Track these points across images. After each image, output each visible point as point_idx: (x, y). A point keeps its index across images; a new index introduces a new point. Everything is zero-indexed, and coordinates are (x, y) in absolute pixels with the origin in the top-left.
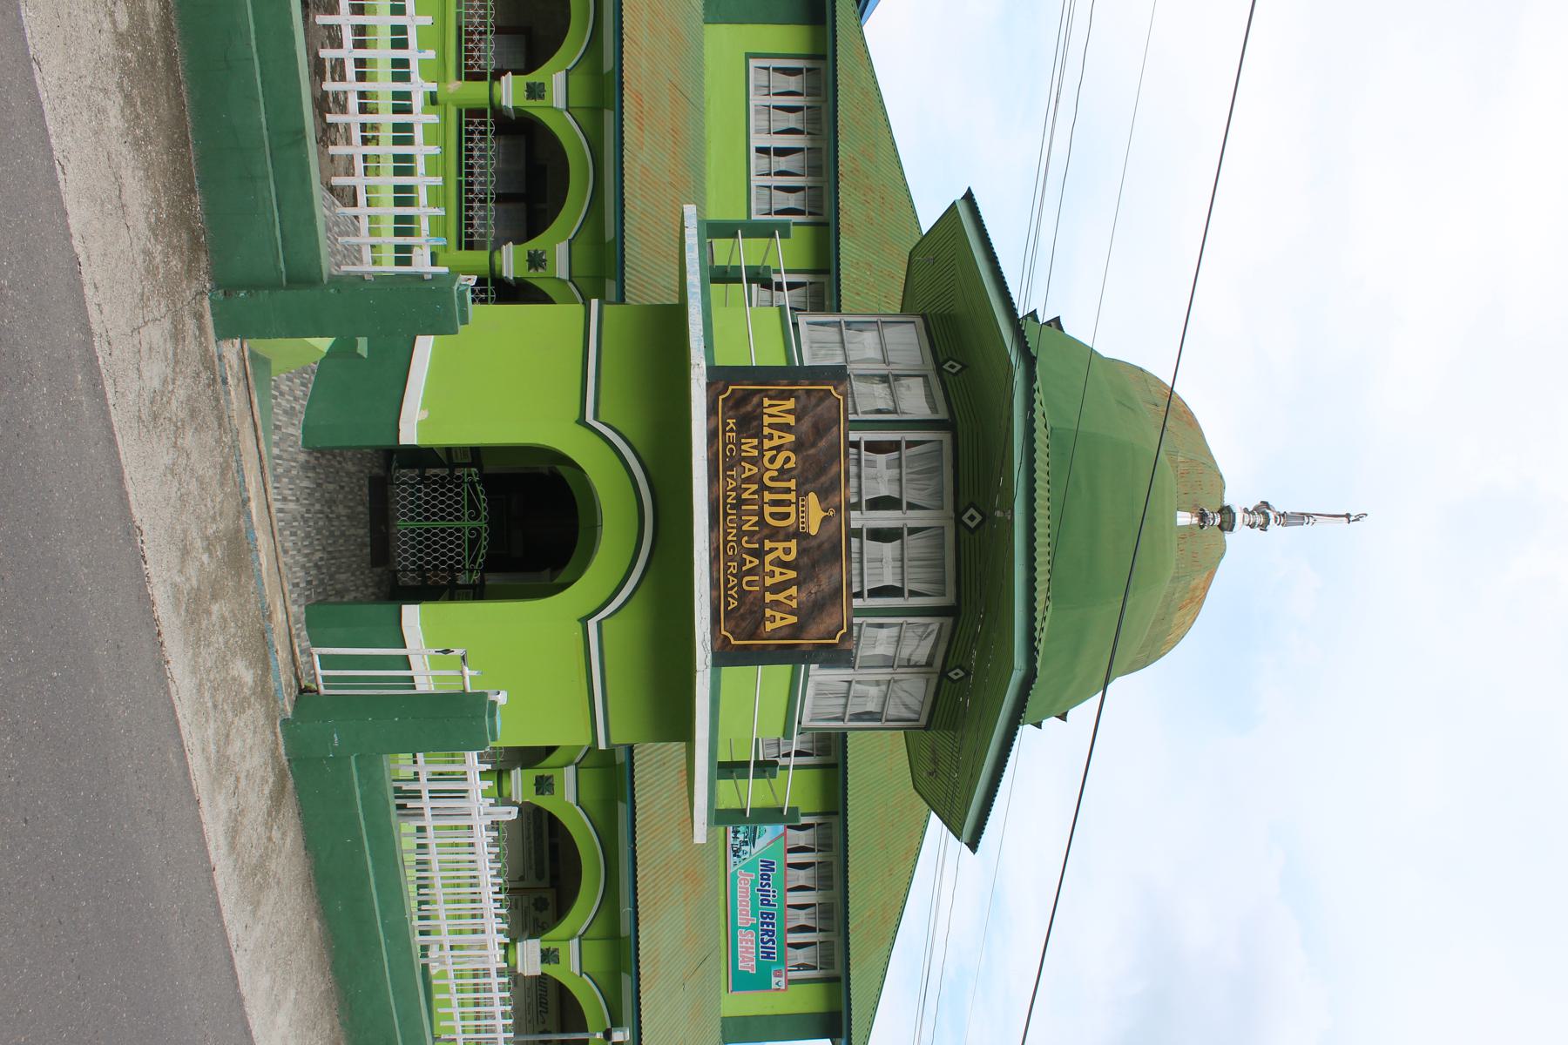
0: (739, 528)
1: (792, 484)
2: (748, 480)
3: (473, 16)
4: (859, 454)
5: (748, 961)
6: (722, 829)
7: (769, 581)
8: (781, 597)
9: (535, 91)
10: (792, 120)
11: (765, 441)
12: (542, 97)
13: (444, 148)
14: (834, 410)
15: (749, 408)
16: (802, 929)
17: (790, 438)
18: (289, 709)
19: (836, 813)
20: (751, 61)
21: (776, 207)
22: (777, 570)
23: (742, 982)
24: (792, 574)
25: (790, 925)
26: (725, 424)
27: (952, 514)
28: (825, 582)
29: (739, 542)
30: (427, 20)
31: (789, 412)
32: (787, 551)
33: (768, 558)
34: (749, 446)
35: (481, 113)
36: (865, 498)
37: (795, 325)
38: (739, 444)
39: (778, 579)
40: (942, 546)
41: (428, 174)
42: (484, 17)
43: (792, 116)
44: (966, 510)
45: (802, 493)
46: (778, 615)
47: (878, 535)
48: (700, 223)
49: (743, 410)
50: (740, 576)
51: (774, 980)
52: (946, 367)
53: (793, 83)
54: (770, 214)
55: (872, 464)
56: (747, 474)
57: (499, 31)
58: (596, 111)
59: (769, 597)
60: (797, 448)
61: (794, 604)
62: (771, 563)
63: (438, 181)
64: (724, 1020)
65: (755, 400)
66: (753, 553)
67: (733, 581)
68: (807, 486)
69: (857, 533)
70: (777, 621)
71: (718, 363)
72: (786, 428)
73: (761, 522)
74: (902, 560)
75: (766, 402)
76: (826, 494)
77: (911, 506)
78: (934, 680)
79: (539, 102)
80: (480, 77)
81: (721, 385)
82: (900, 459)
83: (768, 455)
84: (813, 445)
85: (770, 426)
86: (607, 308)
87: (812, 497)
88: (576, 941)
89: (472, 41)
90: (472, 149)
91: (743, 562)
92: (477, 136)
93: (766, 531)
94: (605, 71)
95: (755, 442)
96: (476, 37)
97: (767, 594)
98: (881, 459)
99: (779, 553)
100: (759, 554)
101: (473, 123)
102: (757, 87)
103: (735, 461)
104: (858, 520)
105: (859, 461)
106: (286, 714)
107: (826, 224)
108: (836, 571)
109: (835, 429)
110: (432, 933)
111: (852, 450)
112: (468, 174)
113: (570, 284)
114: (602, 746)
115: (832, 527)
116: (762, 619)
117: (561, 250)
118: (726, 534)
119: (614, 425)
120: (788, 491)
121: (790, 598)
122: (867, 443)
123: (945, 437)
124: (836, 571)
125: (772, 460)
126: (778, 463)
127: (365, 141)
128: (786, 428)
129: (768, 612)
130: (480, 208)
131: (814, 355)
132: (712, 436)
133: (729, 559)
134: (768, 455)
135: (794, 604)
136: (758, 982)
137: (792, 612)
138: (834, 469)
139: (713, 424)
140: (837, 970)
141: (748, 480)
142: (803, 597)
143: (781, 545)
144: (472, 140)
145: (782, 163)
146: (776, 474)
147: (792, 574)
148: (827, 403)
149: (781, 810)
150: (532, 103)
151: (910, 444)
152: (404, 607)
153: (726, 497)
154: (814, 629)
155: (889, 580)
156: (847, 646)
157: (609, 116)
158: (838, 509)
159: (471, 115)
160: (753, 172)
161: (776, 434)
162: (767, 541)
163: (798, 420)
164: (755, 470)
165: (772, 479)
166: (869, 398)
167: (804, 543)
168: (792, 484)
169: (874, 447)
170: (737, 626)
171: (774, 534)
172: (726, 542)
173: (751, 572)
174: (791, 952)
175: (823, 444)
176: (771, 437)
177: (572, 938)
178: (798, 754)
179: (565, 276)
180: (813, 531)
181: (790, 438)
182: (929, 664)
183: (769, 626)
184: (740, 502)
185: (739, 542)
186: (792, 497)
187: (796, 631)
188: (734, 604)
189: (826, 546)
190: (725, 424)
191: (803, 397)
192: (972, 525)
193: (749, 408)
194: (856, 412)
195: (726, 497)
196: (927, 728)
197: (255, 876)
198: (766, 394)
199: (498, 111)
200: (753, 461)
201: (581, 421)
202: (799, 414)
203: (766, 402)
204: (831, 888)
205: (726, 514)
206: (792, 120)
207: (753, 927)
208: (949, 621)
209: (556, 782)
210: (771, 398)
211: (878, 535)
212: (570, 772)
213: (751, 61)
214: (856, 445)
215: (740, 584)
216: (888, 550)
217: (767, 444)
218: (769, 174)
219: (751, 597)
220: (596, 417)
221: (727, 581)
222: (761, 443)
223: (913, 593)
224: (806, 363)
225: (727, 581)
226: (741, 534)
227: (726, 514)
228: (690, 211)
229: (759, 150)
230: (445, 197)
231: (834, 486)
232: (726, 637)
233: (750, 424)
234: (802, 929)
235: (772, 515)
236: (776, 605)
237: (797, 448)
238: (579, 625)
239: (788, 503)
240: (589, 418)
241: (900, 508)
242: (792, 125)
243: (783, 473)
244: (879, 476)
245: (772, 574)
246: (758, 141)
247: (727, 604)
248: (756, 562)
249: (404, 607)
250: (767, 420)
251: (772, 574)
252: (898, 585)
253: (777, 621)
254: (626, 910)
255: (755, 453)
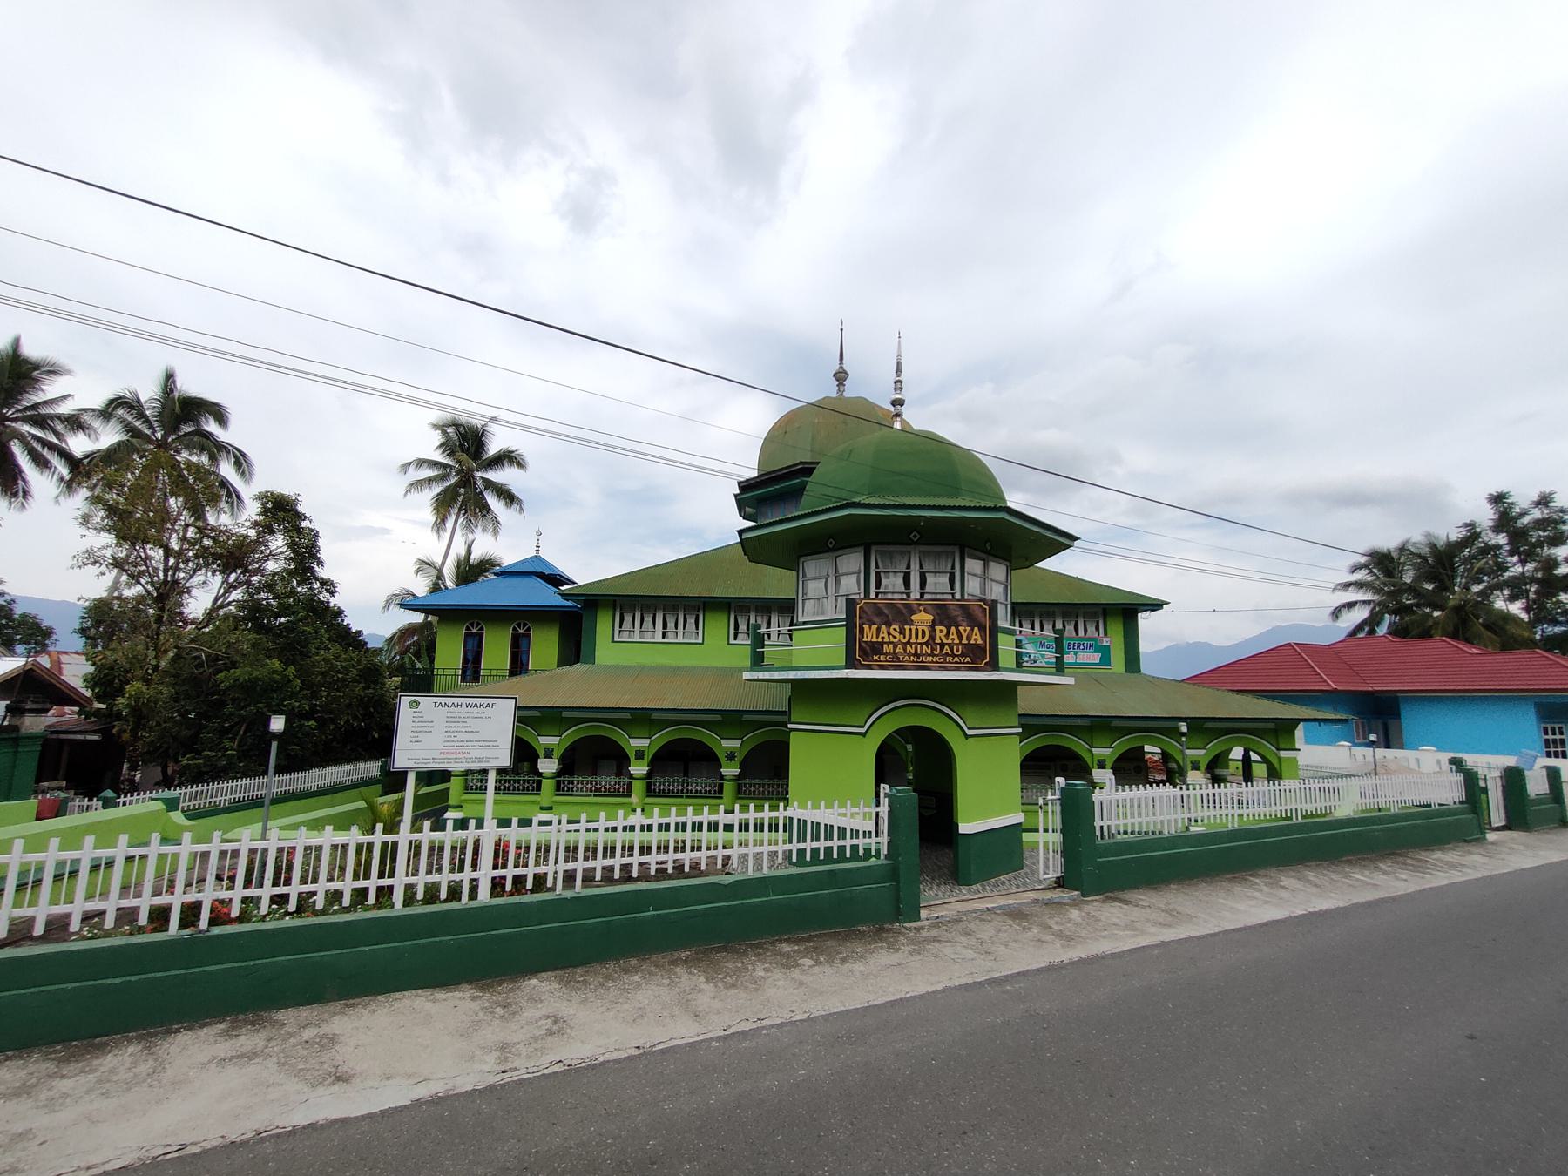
0: (929, 655)
1: (907, 627)
2: (905, 650)
3: (750, 791)
4: (881, 593)
5: (1096, 658)
6: (1066, 670)
7: (957, 641)
8: (965, 635)
9: (640, 755)
10: (648, 619)
11: (885, 640)
12: (643, 751)
13: (674, 805)
14: (869, 605)
15: (868, 648)
16: (1097, 629)
17: (883, 627)
18: (1076, 893)
19: (615, 601)
20: (615, 640)
21: (694, 629)
22: (951, 637)
23: (1106, 661)
24: (953, 629)
25: (1074, 634)
26: (876, 661)
27: (912, 546)
28: (957, 612)
29: (936, 656)
30: (603, 815)
31: (870, 628)
32: (941, 631)
33: (945, 641)
34: (888, 649)
35: (558, 783)
36: (904, 591)
37: (805, 623)
38: (886, 654)
39: (955, 636)
40: (929, 552)
41: (686, 815)
42: (778, 785)
43: (645, 619)
44: (910, 539)
45: (911, 623)
46: (974, 637)
47: (923, 584)
48: (752, 670)
49: (869, 651)
50: (954, 656)
51: (1105, 644)
52: (831, 546)
53: (628, 618)
54: (697, 633)
55: (886, 587)
56: (902, 650)
57: (594, 773)
58: (742, 724)
59: (965, 641)
60: (889, 625)
61: (968, 629)
62: (947, 639)
63: (674, 809)
64: (1126, 671)
65: (864, 645)
66: (942, 650)
67: (956, 659)
68: (908, 620)
69: (922, 595)
70: (977, 637)
71: (844, 664)
72: (878, 630)
73: (926, 644)
74: (936, 573)
75: (865, 639)
76: (911, 610)
77: (908, 567)
78: (991, 557)
79: (646, 753)
80: (721, 787)
81: (856, 662)
82: (884, 572)
83: (892, 639)
84: (887, 616)
85: (877, 637)
86: (792, 720)
87: (913, 618)
88: (1093, 749)
89: (610, 788)
90: (660, 790)
91: (947, 654)
92: (526, 785)
93: (931, 641)
94: (721, 719)
95: (885, 646)
96: (598, 786)
97: (963, 642)
98: (884, 581)
99: (942, 635)
100: (942, 645)
101: (563, 788)
102: (630, 637)
103: (895, 657)
104: (915, 594)
105: (885, 593)
106: (1078, 895)
107: (704, 603)
108: (951, 607)
109: (880, 605)
110: (480, 816)
111: (880, 596)
112: (682, 792)
113: (563, 736)
114: (1020, 730)
115: (929, 608)
116: (976, 645)
117: (725, 743)
118: (932, 662)
119: (867, 716)
120: (910, 630)
121: (965, 631)
122: (876, 588)
123: (874, 548)
124: (951, 607)
125: (895, 637)
126: (897, 634)
127: (747, 845)
128: (878, 630)
129: (972, 642)
130: (692, 786)
131: (841, 612)
132: (882, 667)
133: (945, 662)
134: (892, 639)
135: (968, 629)
136: (1106, 652)
137: (972, 630)
138: (899, 606)
139: (876, 667)
140: (1100, 610)
141: (905, 650)
142: (964, 624)
143: (938, 634)
144: (710, 791)
145: (671, 625)
146: (902, 636)
147: (953, 629)
148: (866, 609)
149: (1056, 638)
150: (646, 757)
151: (877, 567)
152: (960, 832)
153: (913, 662)
154: (981, 619)
155: (945, 579)
156: (990, 602)
157: (655, 716)
158: (920, 605)
159: (650, 790)
160: (652, 640)
161: (881, 635)
162: (936, 641)
163: (874, 624)
164: (899, 646)
165: (904, 637)
166: (851, 585)
167: (937, 622)
168: (907, 627)
169: (878, 585)
170: (979, 658)
171: (932, 637)
172: (937, 662)
173: (952, 650)
174: (1089, 634)
175: (886, 611)
176: (883, 638)
177: (1091, 752)
178: (1033, 628)
179: (740, 741)
180: (932, 618)
181: (883, 627)
182: (984, 560)
183: (980, 642)
184: (916, 654)
185: (936, 656)
186: (914, 628)
187: (982, 628)
188: (968, 659)
189: (939, 611)
190: (876, 661)
191: (864, 620)
192: (918, 536)
193: (868, 648)
194: (859, 594)
195: (913, 662)
196: (1011, 562)
197: (1175, 917)
198: (861, 640)
199: (559, 773)
200: (895, 647)
201: (864, 734)
202: (871, 623)
203: (865, 639)
204: (1054, 612)
205: (922, 662)
206: (648, 619)
207: (1076, 653)
208: (967, 549)
209: (1194, 759)
210: (863, 637)
211: (923, 584)
212: (1188, 752)
213: (615, 640)
214: (877, 594)
215: (958, 656)
216: (930, 579)
217: (886, 640)
218: (677, 632)
219: (964, 650)
220: (863, 727)
221: (956, 662)
222: (886, 643)
223: (953, 568)
224: (844, 616)
225: (956, 662)
226: (933, 655)
227: (922, 662)
228: (747, 675)
229: (663, 637)
230: (681, 805)
231: (908, 607)
232: (986, 664)
233: (876, 648)
234: (1097, 629)
235: (923, 638)
236: (968, 638)
237: (889, 625)
238: (969, 739)
239: (917, 630)
240: (863, 730)
241: (954, 573)
242: (651, 619)
243: (902, 632)
244: (893, 584)
245: (953, 639)
246: (659, 638)
247: (968, 663)
248: (946, 647)
249: (960, 832)
250: (874, 640)
251: (953, 639)
252: (902, 575)
253: (977, 637)
254: (1079, 722)
255: (891, 646)
